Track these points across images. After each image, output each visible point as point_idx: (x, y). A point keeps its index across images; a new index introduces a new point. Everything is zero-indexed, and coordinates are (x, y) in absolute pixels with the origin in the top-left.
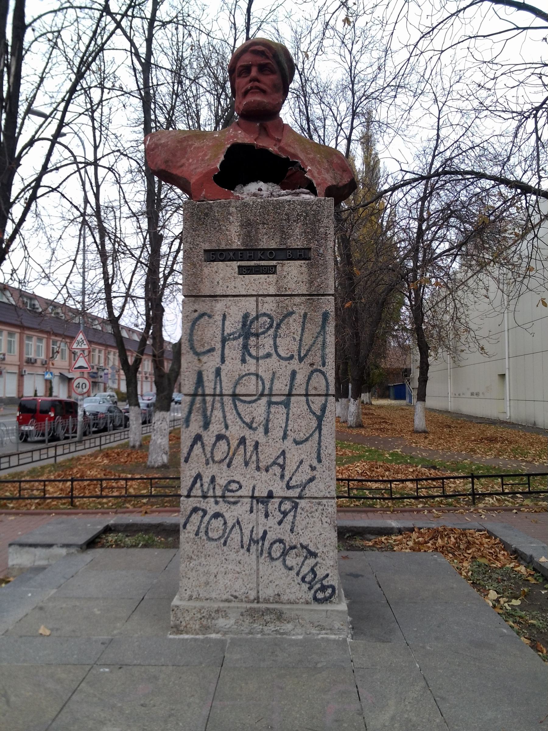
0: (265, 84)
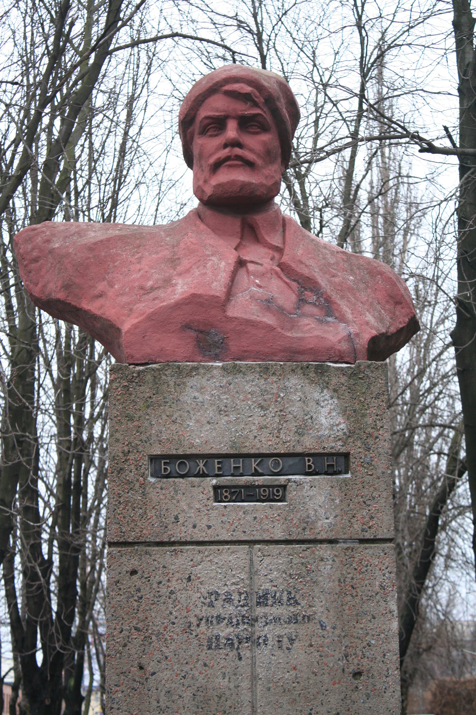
0: (251, 150)
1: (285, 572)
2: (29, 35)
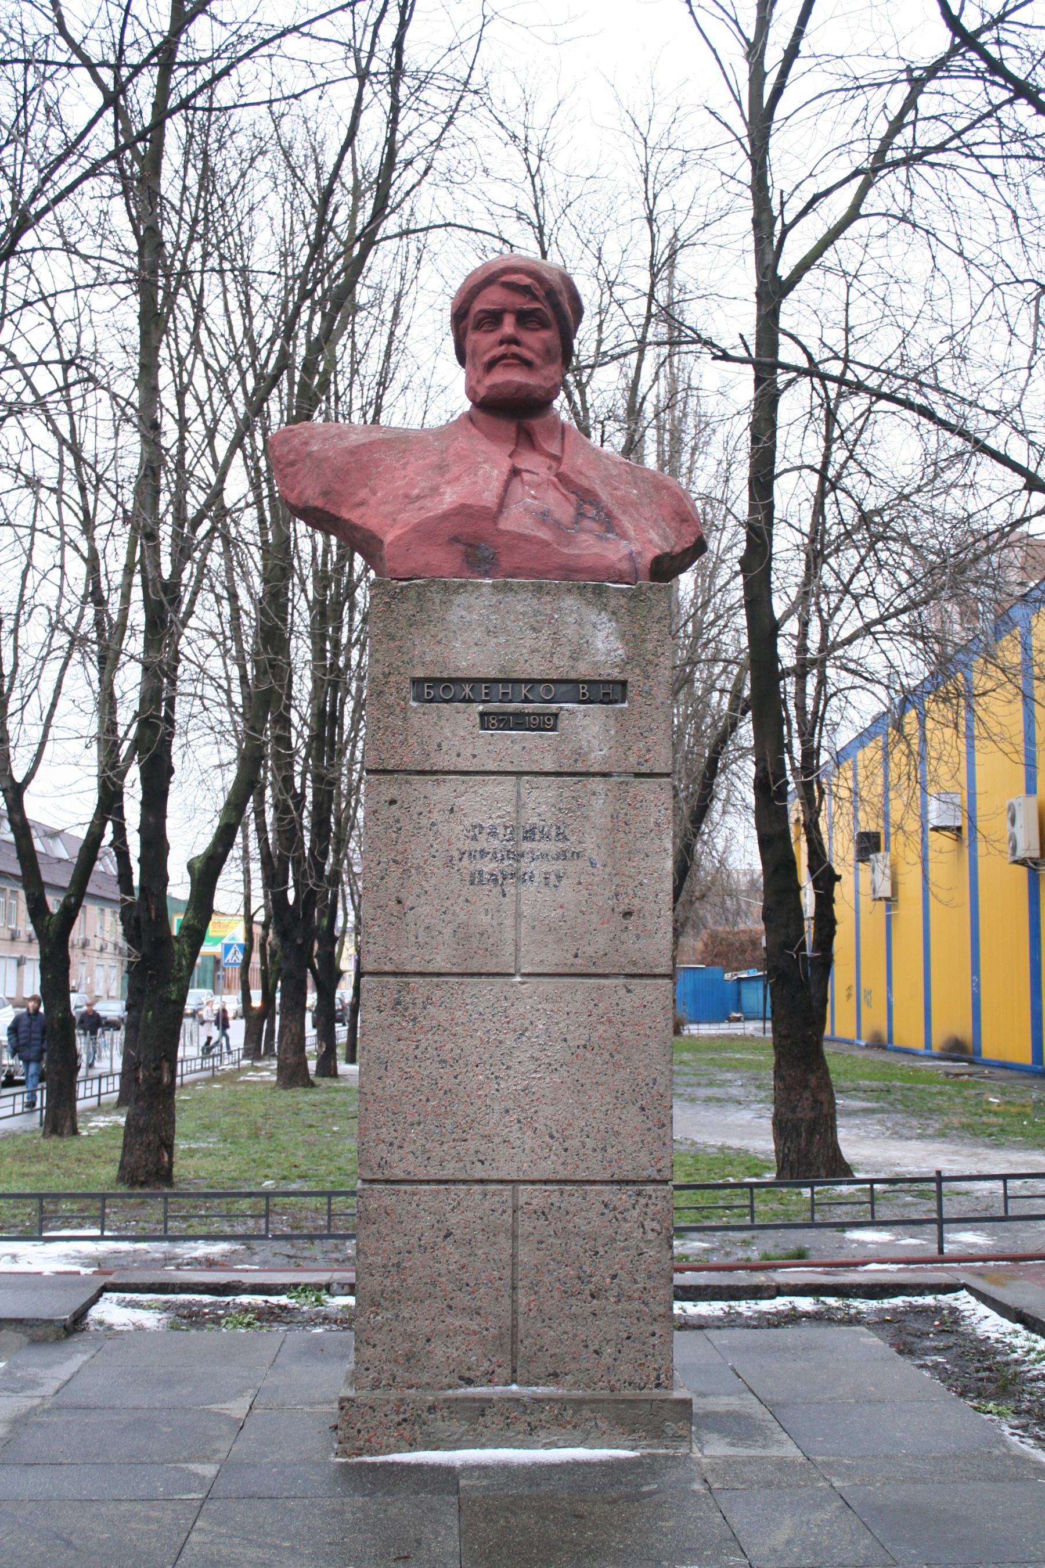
0: (530, 348)
1: (554, 806)
2: (288, 222)
